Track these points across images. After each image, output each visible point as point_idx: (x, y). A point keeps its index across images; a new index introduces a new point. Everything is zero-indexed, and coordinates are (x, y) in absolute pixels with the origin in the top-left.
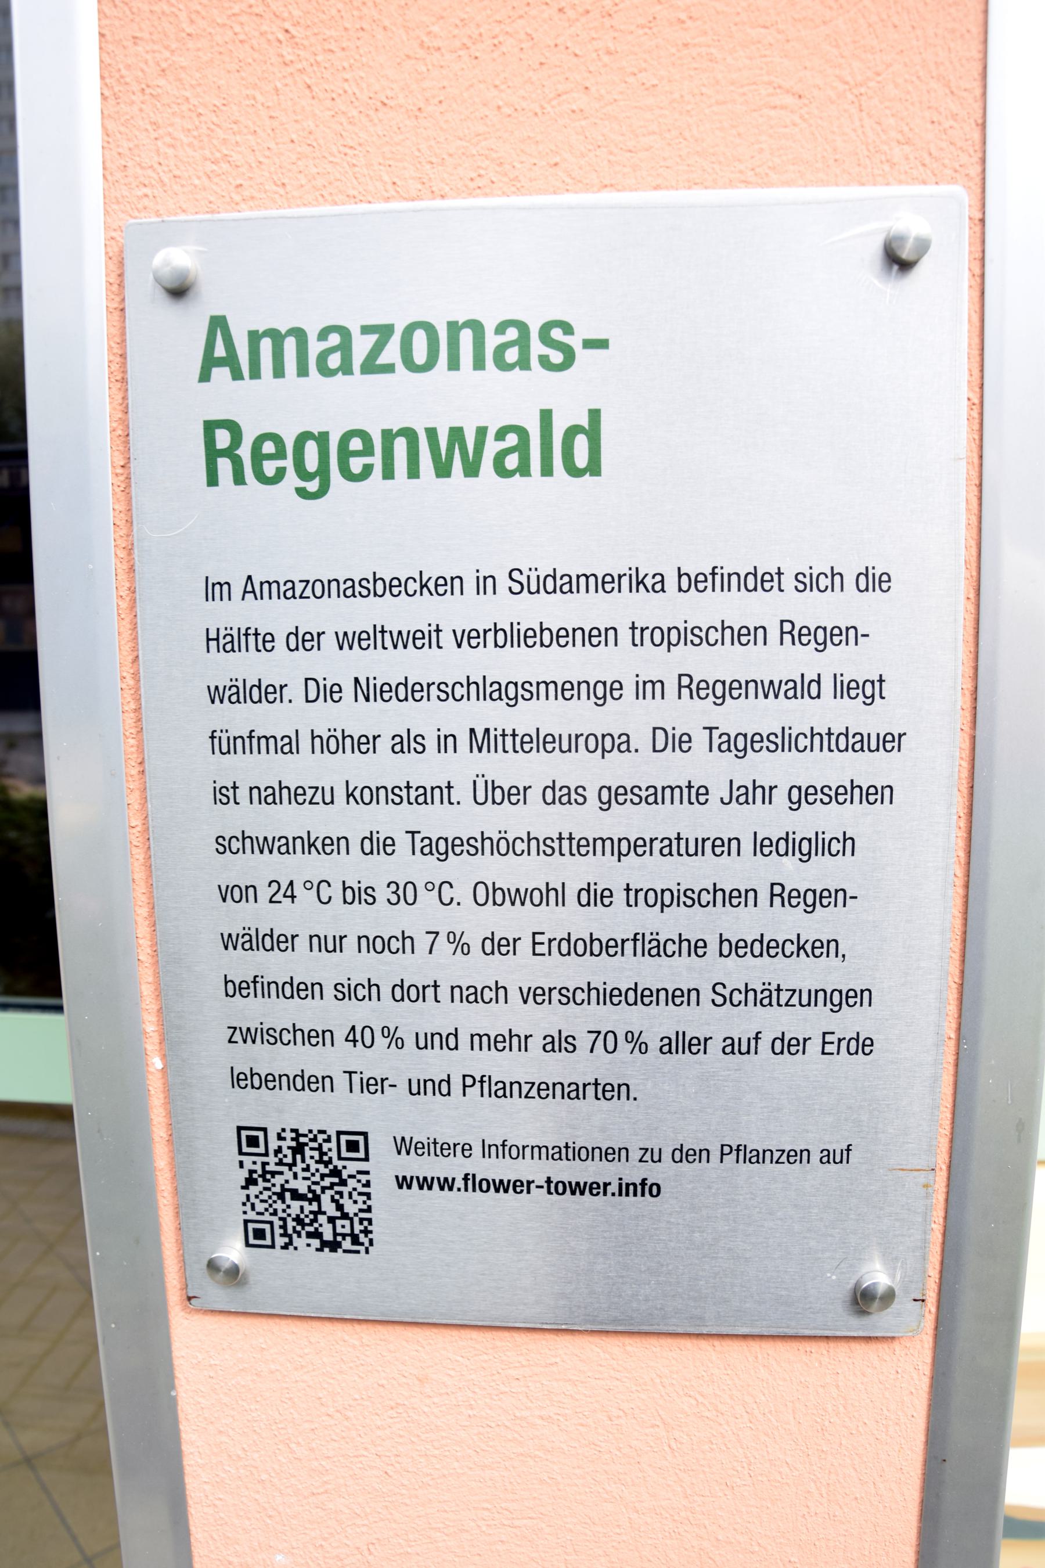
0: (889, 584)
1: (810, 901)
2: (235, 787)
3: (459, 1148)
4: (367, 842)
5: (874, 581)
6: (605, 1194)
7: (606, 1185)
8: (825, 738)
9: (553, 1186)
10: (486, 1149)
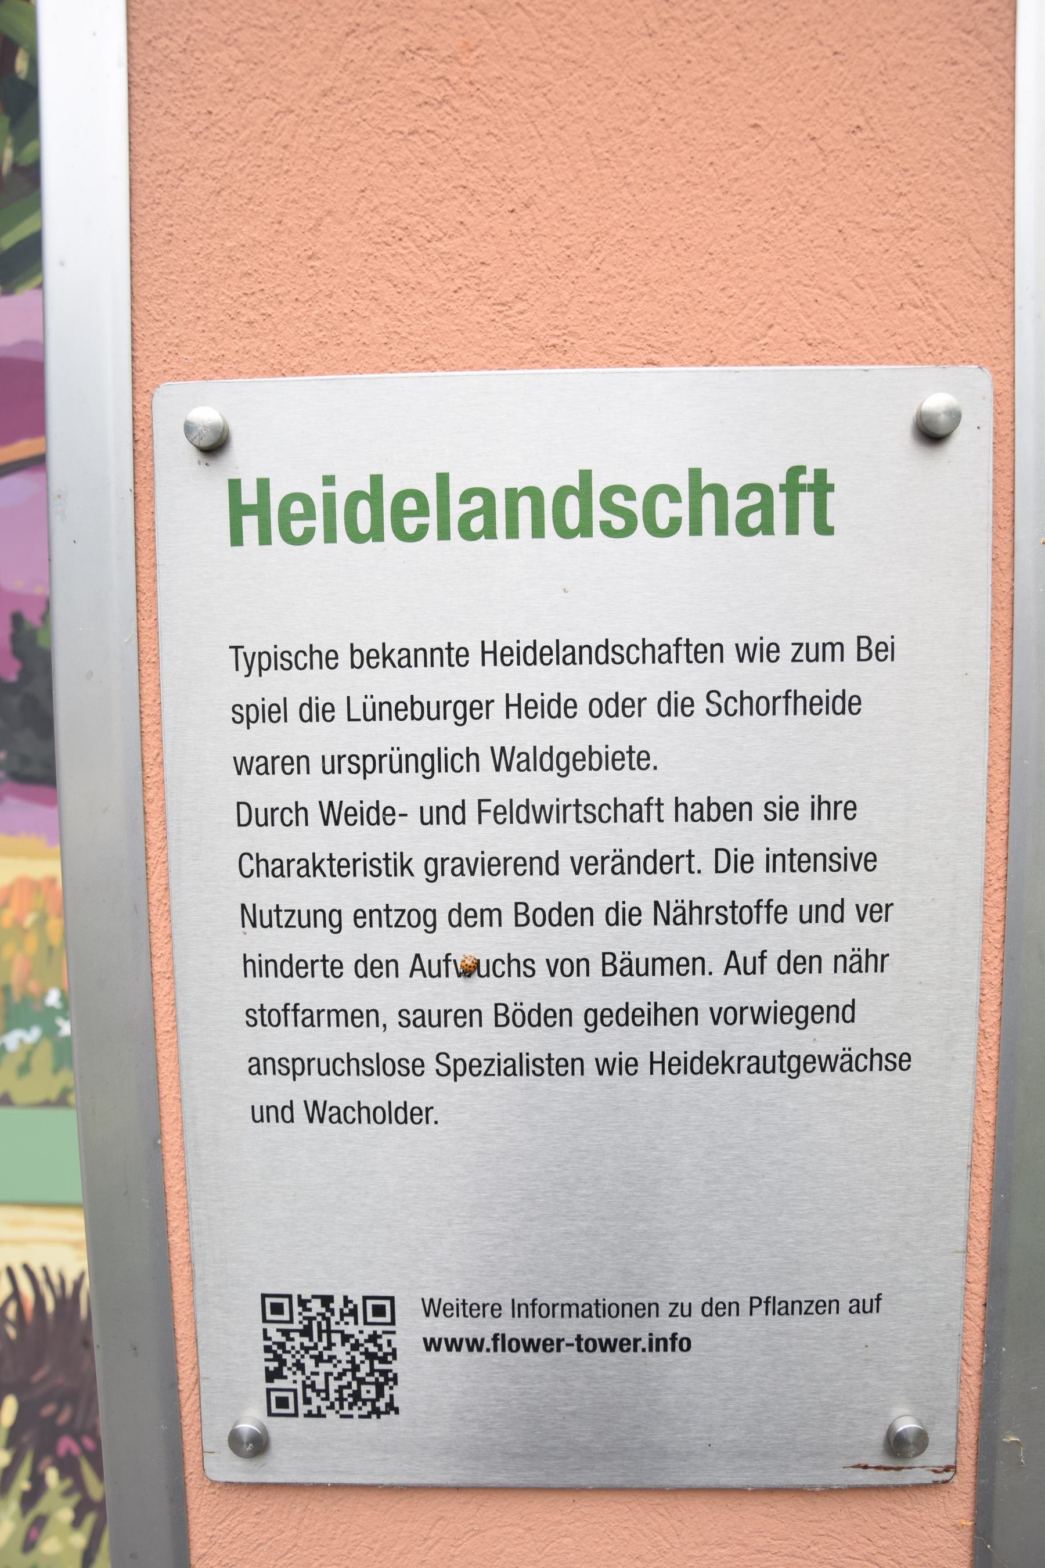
0: (336, 661)
1: (802, 1018)
3: (488, 1309)
5: (875, 650)
6: (635, 1350)
7: (636, 1341)
10: (516, 1309)
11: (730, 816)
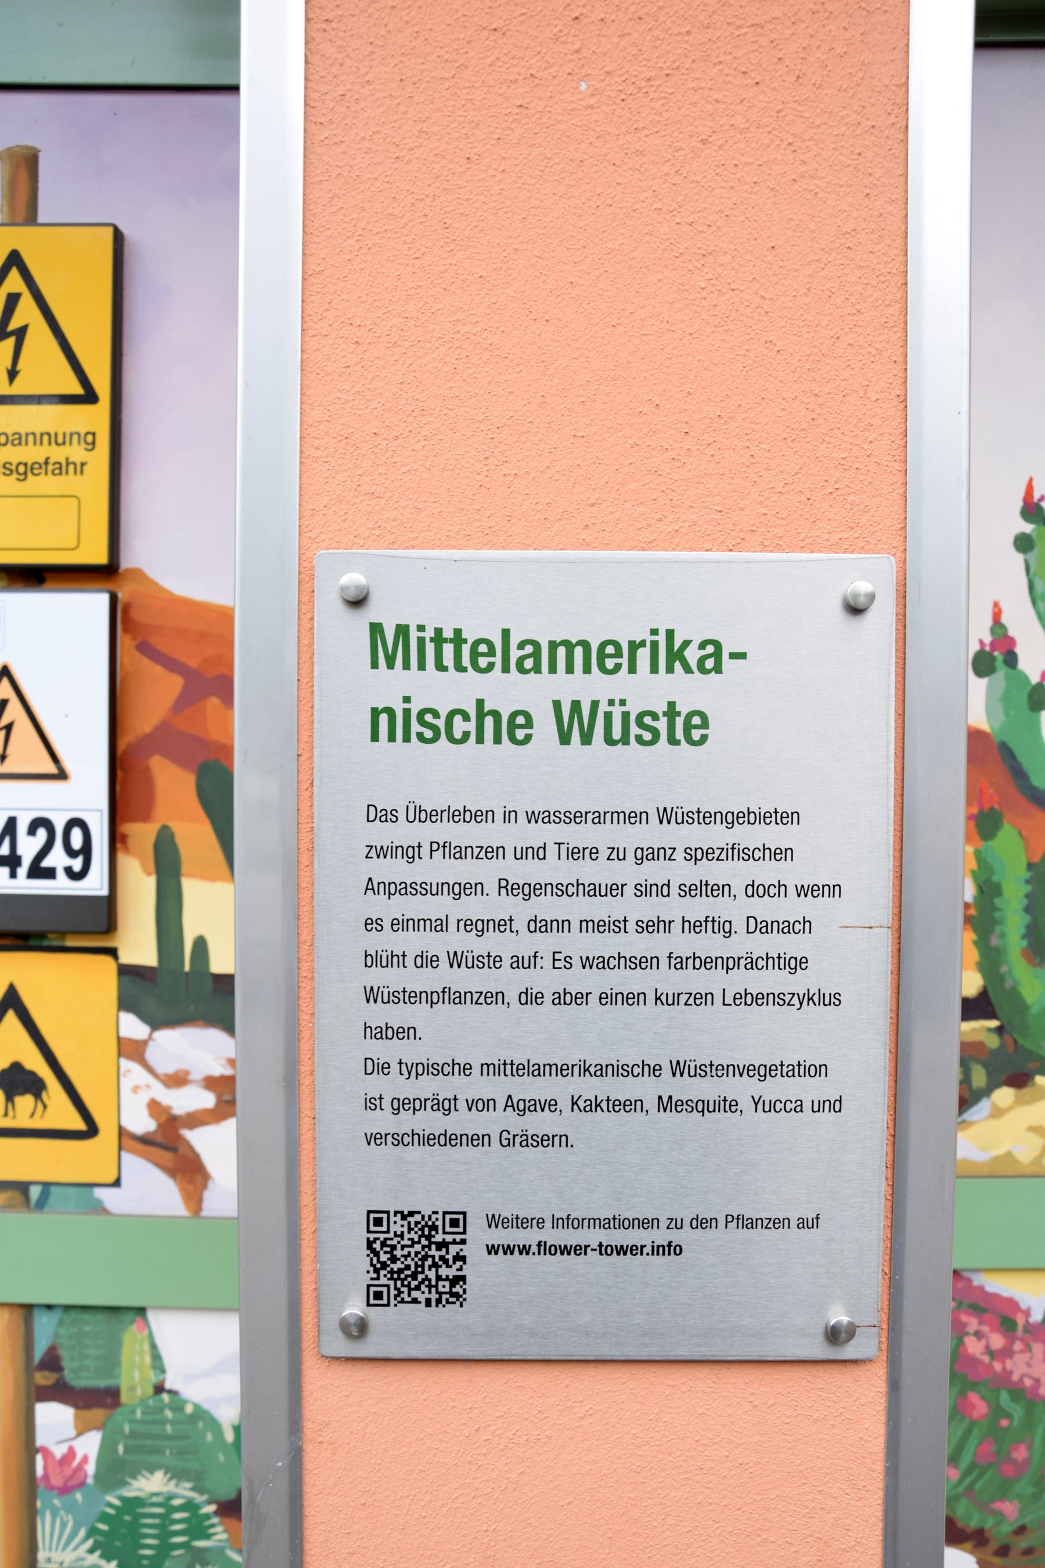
2: (381, 1098)
4: (523, 995)
6: (642, 1254)
7: (642, 1247)
8: (776, 960)
9: (603, 1249)
10: (556, 1222)
11: (401, 1036)
